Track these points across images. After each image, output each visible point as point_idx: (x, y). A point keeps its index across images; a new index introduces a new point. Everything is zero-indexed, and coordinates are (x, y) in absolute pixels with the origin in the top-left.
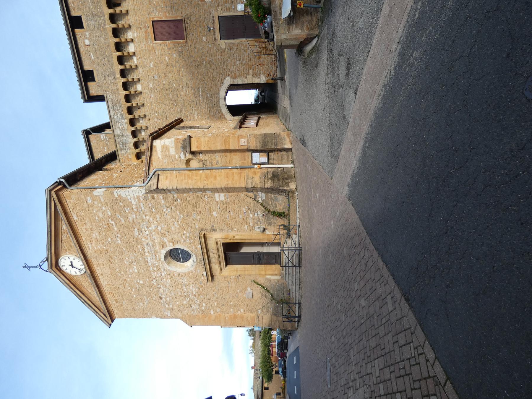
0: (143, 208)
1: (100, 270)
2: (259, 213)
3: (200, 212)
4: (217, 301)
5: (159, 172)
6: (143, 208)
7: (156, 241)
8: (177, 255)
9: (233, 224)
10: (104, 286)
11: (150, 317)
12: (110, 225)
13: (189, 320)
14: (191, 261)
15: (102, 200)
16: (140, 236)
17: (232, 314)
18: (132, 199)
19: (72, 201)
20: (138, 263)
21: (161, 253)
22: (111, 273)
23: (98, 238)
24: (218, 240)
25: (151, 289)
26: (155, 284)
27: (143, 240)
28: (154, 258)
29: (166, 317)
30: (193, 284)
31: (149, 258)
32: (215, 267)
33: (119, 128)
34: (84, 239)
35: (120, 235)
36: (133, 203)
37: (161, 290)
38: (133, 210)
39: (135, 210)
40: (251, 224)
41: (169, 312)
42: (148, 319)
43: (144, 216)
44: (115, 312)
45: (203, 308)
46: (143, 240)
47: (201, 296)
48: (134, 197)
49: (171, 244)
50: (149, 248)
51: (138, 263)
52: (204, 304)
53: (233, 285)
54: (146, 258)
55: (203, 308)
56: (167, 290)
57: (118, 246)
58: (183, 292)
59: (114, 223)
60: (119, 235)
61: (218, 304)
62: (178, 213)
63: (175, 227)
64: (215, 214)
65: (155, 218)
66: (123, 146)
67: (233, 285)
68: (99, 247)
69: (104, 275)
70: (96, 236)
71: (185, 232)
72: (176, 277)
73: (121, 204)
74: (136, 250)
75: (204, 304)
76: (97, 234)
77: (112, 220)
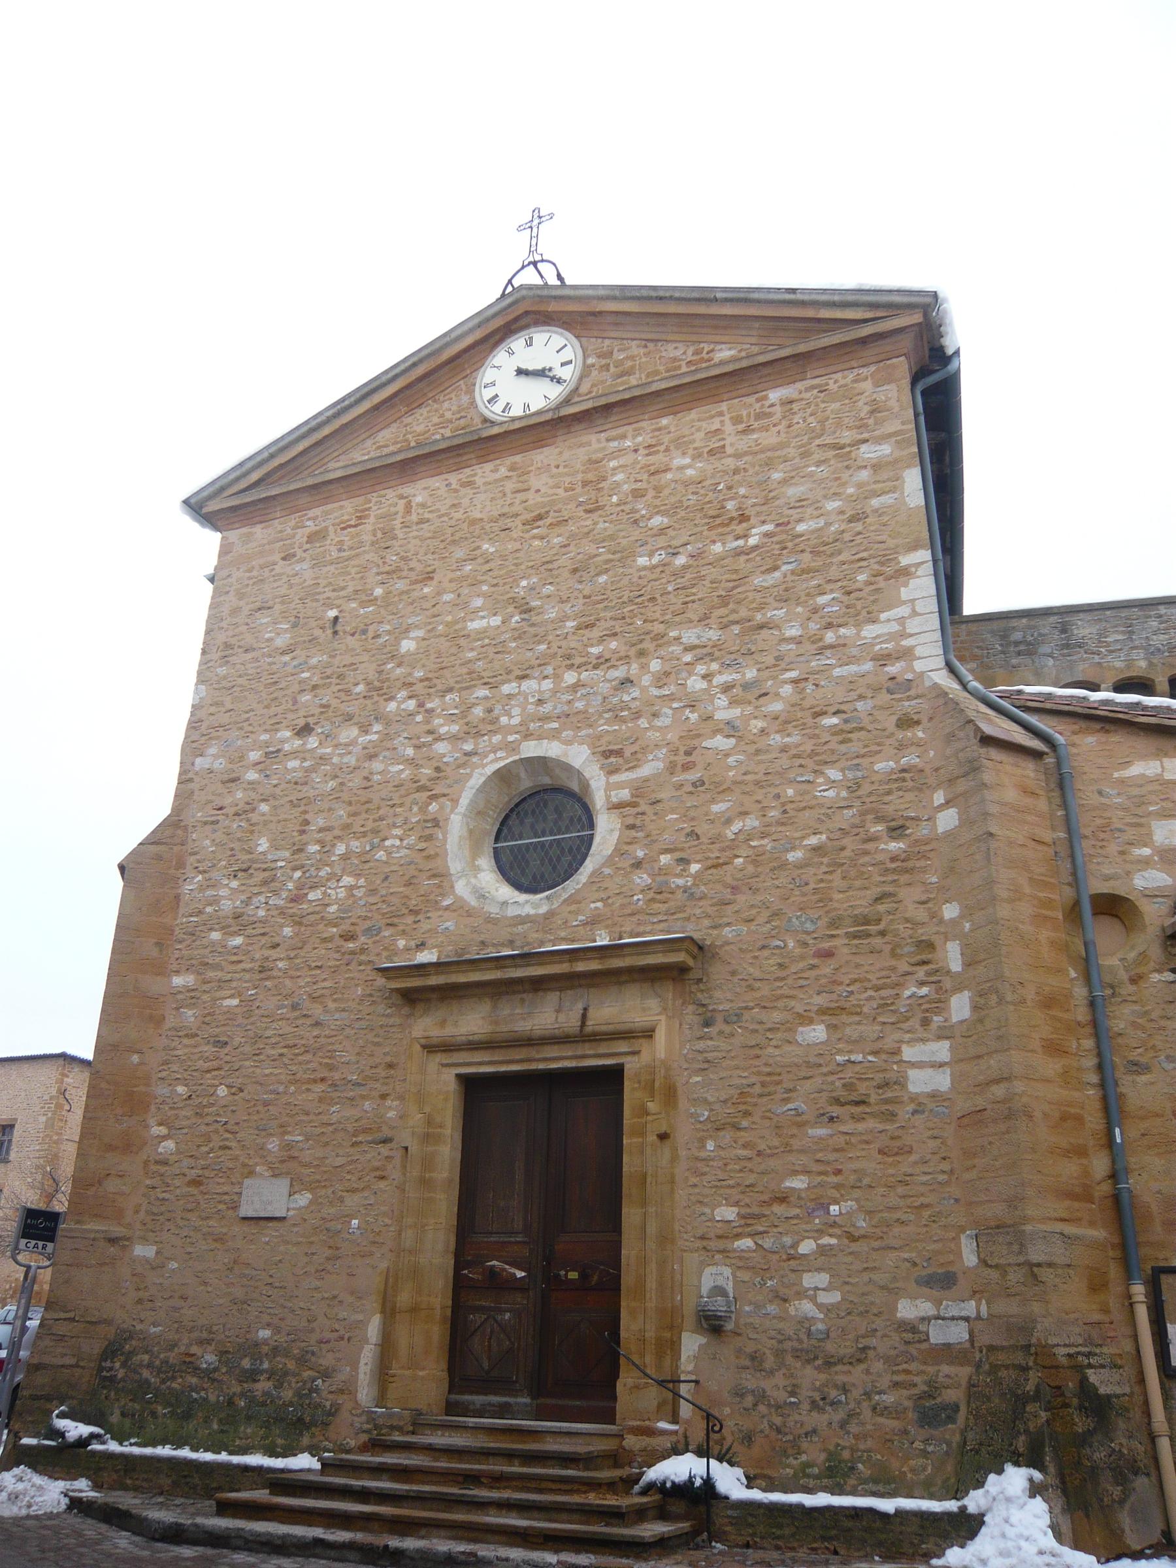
0: (837, 672)
1: (492, 477)
2: (825, 1298)
3: (829, 954)
4: (248, 1014)
5: (1050, 760)
6: (837, 672)
7: (643, 723)
8: (538, 824)
9: (745, 1136)
10: (407, 490)
11: (202, 679)
12: (740, 529)
13: (159, 858)
14: (505, 892)
15: (875, 502)
16: (676, 649)
17: (162, 1090)
18: (894, 627)
19: (867, 386)
20: (519, 636)
21: (568, 743)
22: (473, 522)
23: (669, 476)
24: (643, 1045)
25: (361, 688)
26: (392, 706)
27: (655, 665)
28: (547, 708)
29: (192, 748)
30: (373, 892)
31: (547, 685)
32: (471, 1021)
33: (1102, 634)
34: (664, 421)
35: (685, 567)
36: (870, 631)
37: (355, 731)
38: (829, 626)
39: (830, 637)
40: (746, 1243)
41: (220, 764)
42: (195, 667)
43: (793, 674)
44: (258, 530)
45: (215, 936)
46: (655, 665)
47: (288, 931)
48: (904, 635)
49: (625, 794)
50: (604, 688)
51: (519, 636)
52: (238, 941)
53: (336, 1112)
54: (549, 670)
55: (215, 936)
56: (351, 760)
57: (626, 556)
58: (328, 837)
59: (752, 541)
60: (681, 560)
61: (230, 1013)
62: (813, 841)
63: (728, 822)
64: (817, 1033)
65: (783, 723)
66: (1017, 643)
67: (336, 1112)
68: (619, 477)
69: (469, 491)
70: (682, 468)
71: (695, 868)
72: (423, 809)
73: (862, 578)
74: (596, 633)
75: (238, 941)
76: (690, 472)
77: (767, 535)
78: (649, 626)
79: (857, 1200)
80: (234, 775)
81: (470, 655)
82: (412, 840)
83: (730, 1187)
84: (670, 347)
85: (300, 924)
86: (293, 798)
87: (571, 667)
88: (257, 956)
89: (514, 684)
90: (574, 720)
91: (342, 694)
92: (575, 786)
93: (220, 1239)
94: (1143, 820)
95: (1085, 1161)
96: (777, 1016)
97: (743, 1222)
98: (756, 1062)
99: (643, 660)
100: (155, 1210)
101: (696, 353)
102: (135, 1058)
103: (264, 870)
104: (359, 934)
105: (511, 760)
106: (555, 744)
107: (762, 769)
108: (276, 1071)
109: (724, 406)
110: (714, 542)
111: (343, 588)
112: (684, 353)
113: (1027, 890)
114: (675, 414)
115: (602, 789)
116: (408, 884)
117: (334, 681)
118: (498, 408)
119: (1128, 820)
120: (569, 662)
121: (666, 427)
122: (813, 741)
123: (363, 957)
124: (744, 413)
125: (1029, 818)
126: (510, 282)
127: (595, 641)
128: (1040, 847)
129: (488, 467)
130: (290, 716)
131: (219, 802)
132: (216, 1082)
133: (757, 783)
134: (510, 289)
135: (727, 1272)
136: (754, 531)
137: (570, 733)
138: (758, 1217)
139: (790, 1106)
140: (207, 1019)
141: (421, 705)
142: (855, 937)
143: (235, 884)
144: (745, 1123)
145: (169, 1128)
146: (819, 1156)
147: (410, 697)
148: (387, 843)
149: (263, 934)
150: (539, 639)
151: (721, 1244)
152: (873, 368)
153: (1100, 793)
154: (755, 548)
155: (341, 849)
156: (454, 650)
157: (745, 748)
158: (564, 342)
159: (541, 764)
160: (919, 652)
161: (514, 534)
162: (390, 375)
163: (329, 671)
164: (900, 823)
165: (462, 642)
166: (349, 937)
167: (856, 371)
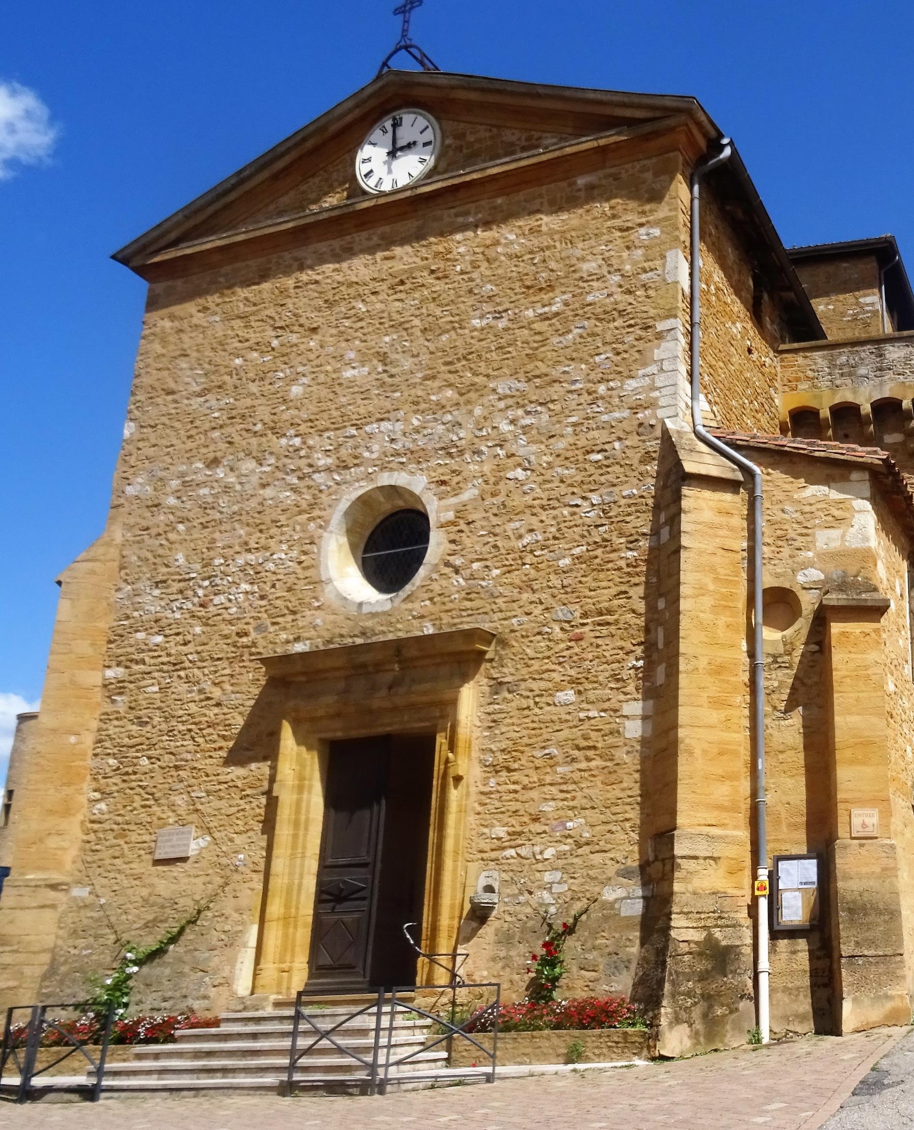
2: (556, 889)
9: (516, 776)
19: (648, 175)
31: (399, 426)
34: (499, 201)
45: (141, 636)
49: (451, 515)
58: (229, 552)
62: (576, 551)
78: (476, 379)
79: (585, 817)
80: (156, 502)
81: (343, 400)
82: (294, 554)
83: (503, 813)
84: (508, 132)
85: (207, 625)
86: (203, 520)
87: (416, 412)
88: (173, 652)
89: (375, 426)
90: (417, 457)
91: (244, 433)
92: (420, 508)
93: (138, 878)
94: (809, 531)
95: (736, 783)
96: (543, 685)
97: (509, 838)
98: (526, 720)
99: (470, 407)
100: (89, 859)
101: (528, 139)
102: (73, 739)
103: (180, 581)
104: (251, 630)
105: (370, 488)
106: (403, 474)
107: (545, 495)
108: (185, 743)
109: (544, 189)
110: (527, 309)
111: (247, 340)
112: (519, 139)
113: (711, 587)
114: (508, 195)
115: (437, 511)
116: (289, 590)
117: (238, 420)
118: (372, 182)
119: (799, 531)
120: (415, 408)
121: (500, 206)
122: (583, 473)
123: (253, 650)
124: (558, 196)
125: (721, 533)
126: (385, 64)
127: (435, 391)
128: (730, 554)
129: (364, 234)
130: (204, 450)
131: (145, 523)
132: (139, 755)
133: (543, 507)
134: (386, 69)
135: (495, 874)
136: (558, 299)
137: (414, 466)
138: (520, 834)
139: (547, 751)
140: (133, 705)
141: (304, 443)
142: (599, 625)
143: (157, 592)
144: (516, 766)
145: (103, 793)
146: (564, 787)
147: (296, 436)
148: (275, 557)
149: (178, 634)
150: (395, 388)
151: (494, 855)
152: (654, 160)
153: (783, 511)
154: (557, 314)
155: (240, 561)
156: (331, 396)
157: (537, 479)
158: (426, 123)
159: (394, 490)
160: (662, 402)
161: (380, 297)
162: (284, 148)
163: (234, 413)
164: (636, 537)
165: (337, 389)
166: (242, 634)
167: (643, 162)
